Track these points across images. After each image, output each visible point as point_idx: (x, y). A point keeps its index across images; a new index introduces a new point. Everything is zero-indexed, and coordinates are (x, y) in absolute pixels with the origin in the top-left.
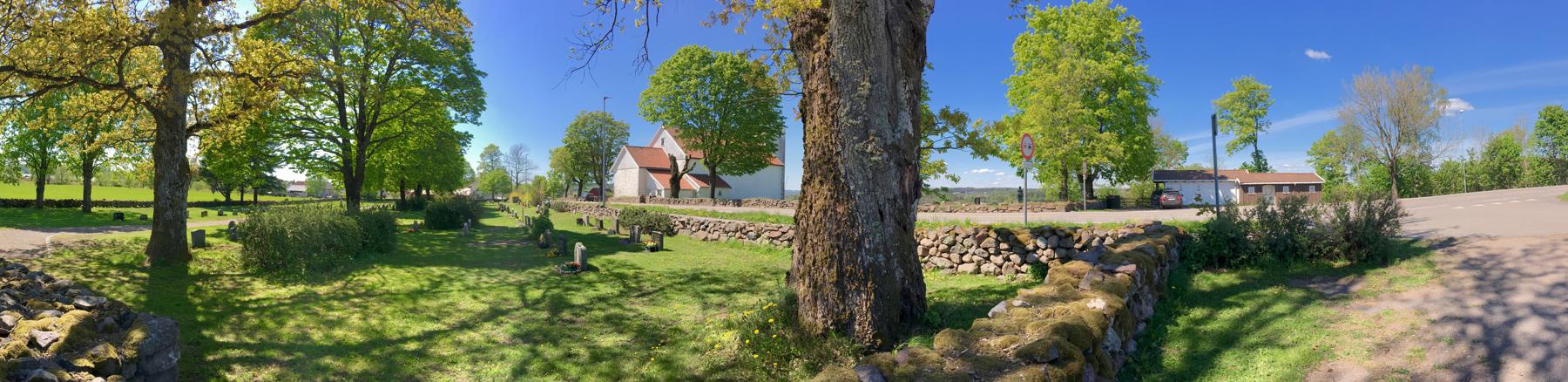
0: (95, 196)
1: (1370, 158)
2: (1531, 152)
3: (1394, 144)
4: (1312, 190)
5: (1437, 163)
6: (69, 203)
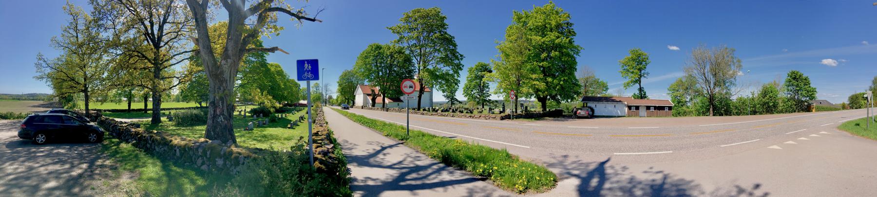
0: (132, 108)
1: (698, 93)
2: (783, 94)
3: (712, 86)
4: (667, 110)
5: (734, 98)
6: (140, 110)
